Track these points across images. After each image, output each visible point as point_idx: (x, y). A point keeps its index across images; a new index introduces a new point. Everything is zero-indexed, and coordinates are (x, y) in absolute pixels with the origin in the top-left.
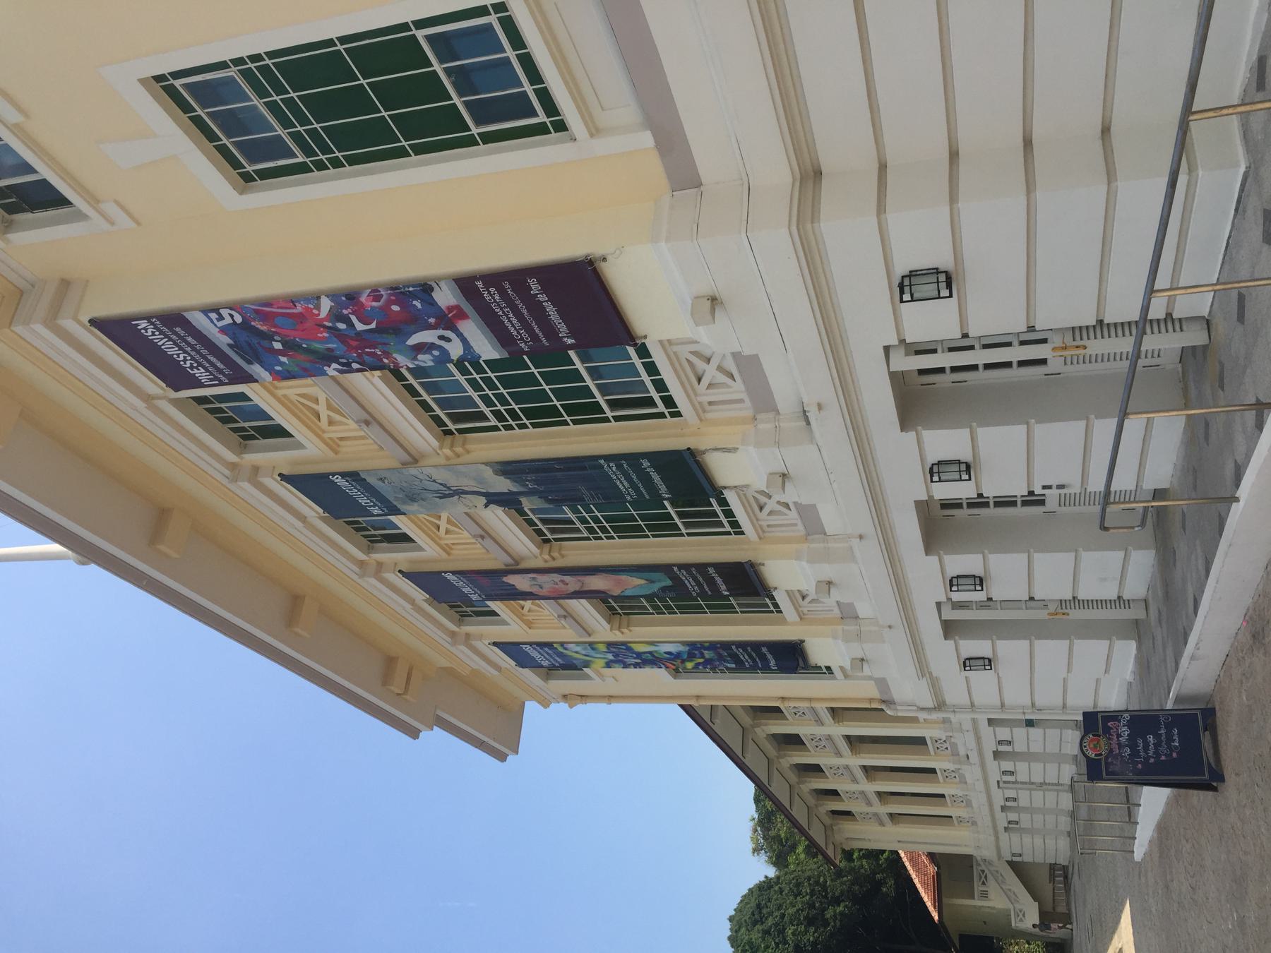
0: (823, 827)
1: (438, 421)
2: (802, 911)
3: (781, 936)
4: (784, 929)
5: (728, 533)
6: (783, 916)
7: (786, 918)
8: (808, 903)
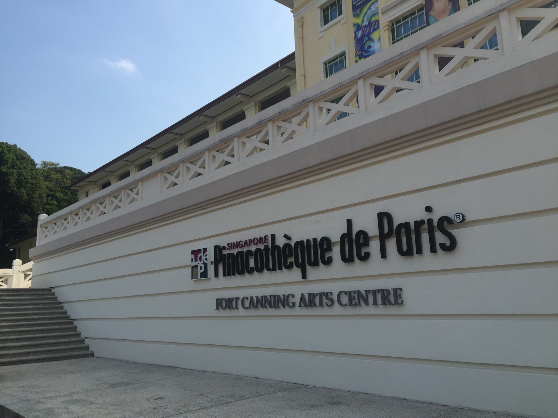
0: (133, 161)
2: (24, 178)
3: (11, 167)
5: (345, 57)
6: (21, 169)
7: (20, 170)
8: (28, 181)
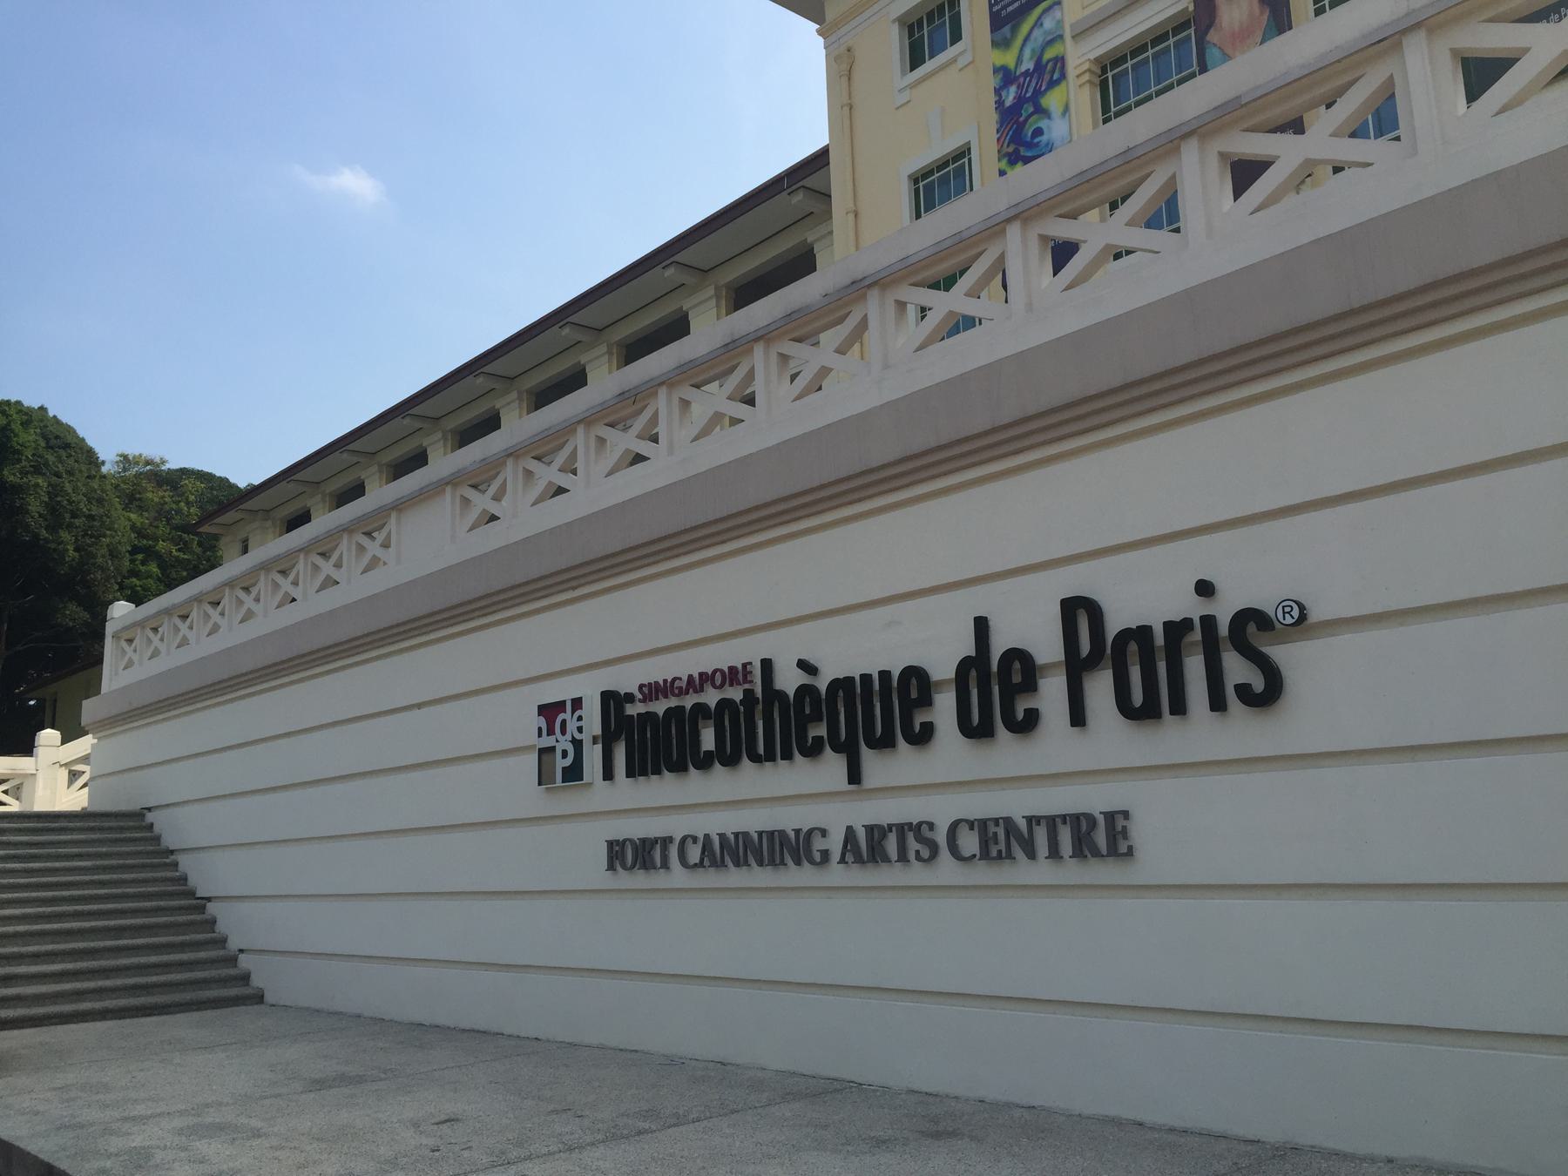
0: (373, 452)
1: (930, 173)
2: (68, 500)
3: (32, 469)
4: (40, 474)
6: (58, 475)
7: (56, 478)
8: (78, 510)
